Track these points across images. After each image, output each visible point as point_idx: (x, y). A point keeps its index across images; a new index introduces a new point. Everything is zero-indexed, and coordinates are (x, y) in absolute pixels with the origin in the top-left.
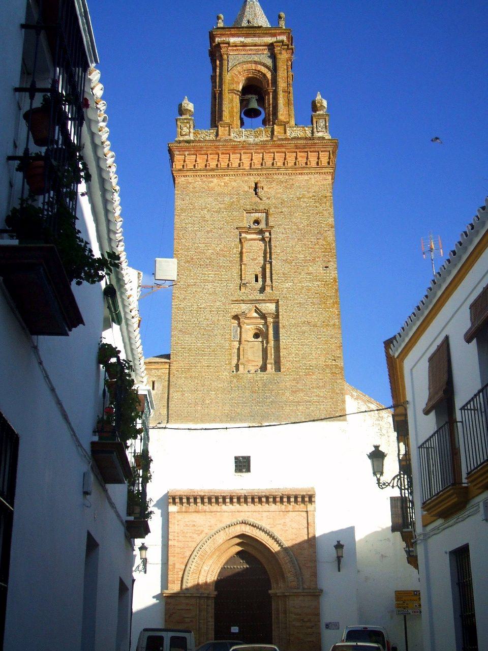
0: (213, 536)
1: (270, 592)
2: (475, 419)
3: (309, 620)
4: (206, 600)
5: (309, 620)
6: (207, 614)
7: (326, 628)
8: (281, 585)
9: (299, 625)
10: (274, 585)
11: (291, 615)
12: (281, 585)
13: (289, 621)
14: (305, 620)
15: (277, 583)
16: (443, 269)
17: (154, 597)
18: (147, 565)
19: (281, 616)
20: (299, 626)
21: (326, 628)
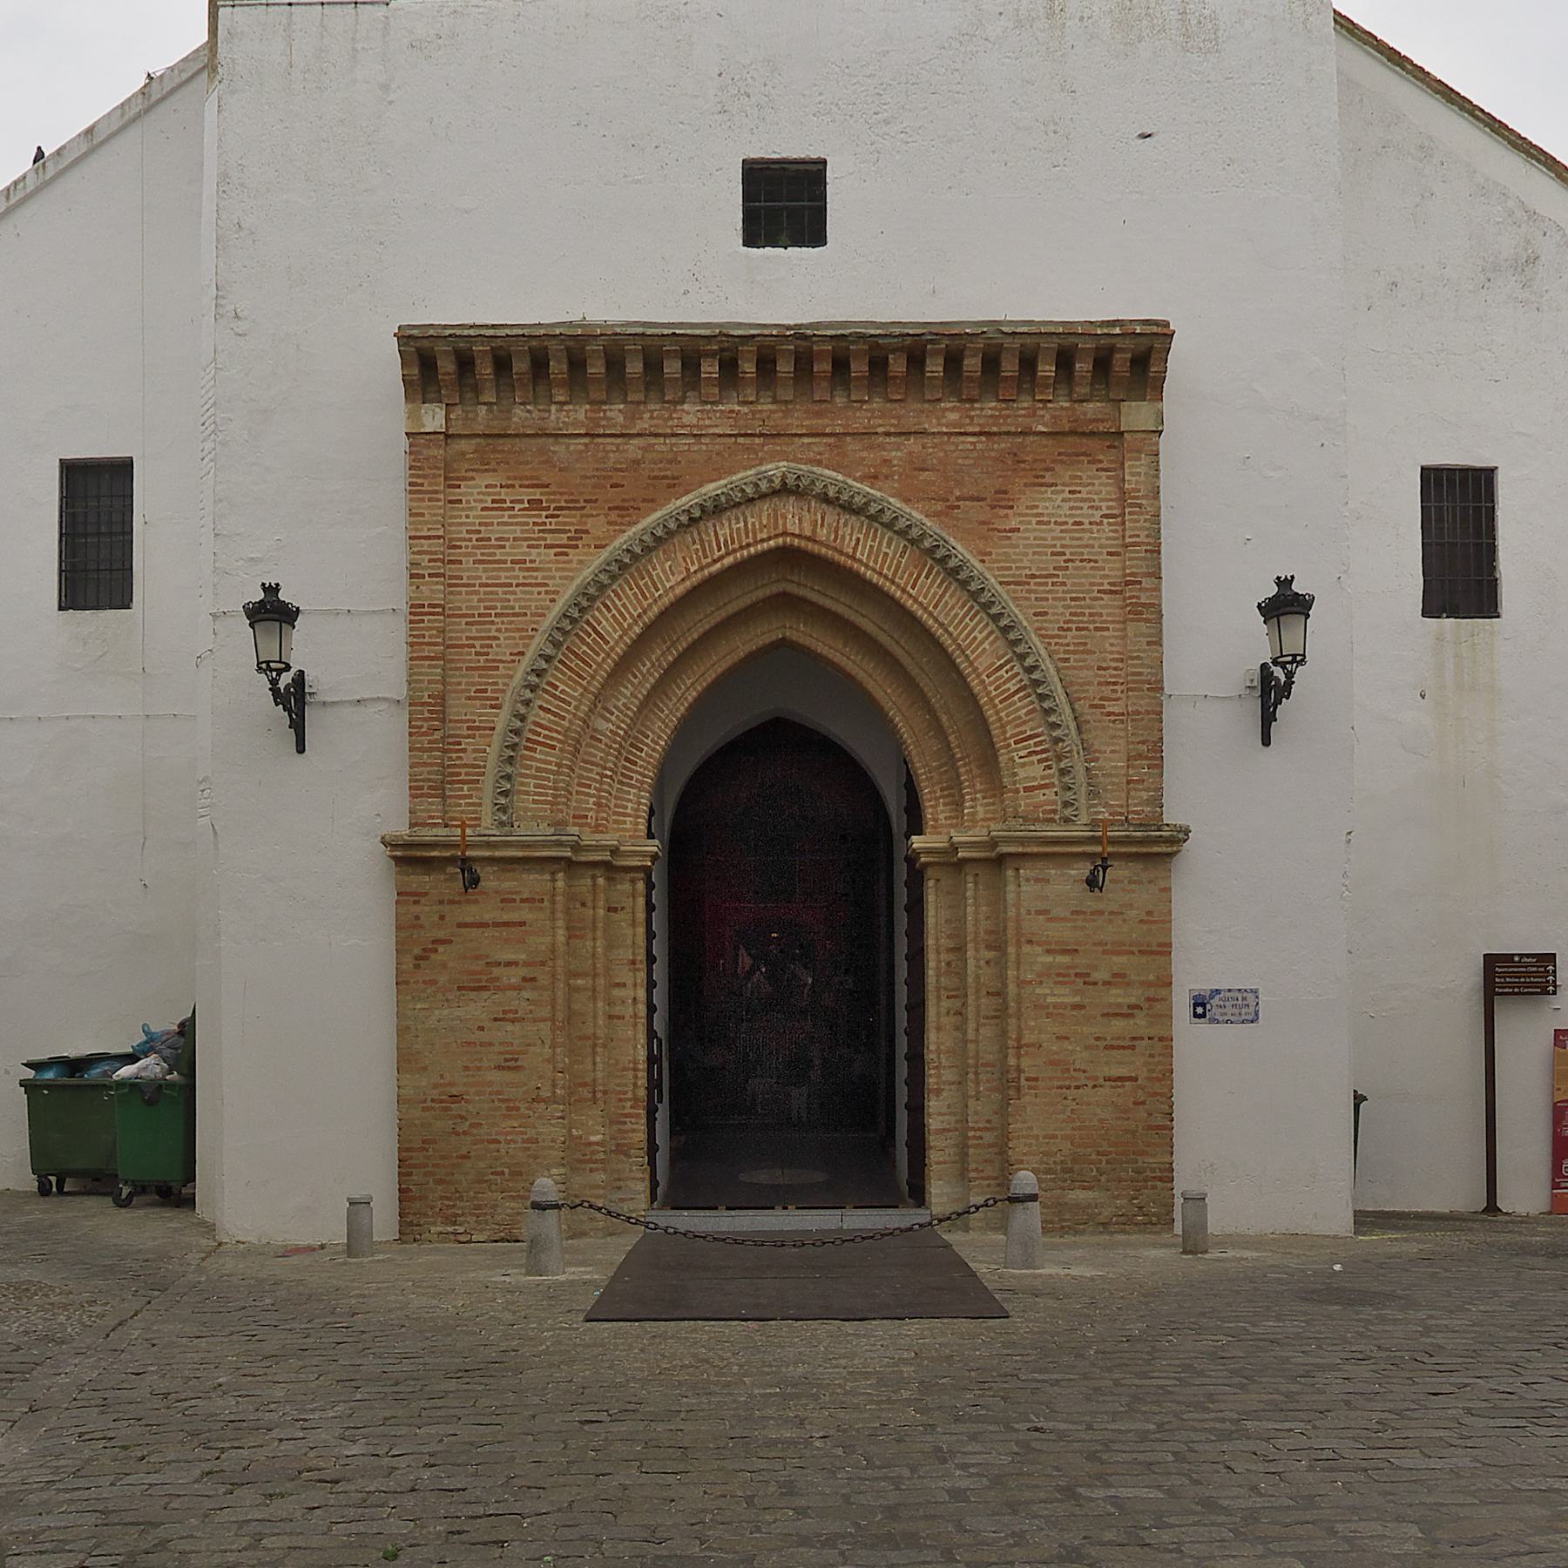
0: (523, 718)
1: (917, 842)
2: (1260, 1340)
3: (1119, 978)
4: (601, 881)
5: (1119, 978)
6: (610, 947)
7: (1196, 1015)
8: (978, 806)
9: (1069, 1000)
10: (935, 809)
11: (1026, 949)
12: (978, 806)
13: (1020, 983)
14: (1096, 976)
15: (958, 804)
16: (624, 496)
17: (28, 1065)
18: (309, 713)
19: (976, 958)
20: (1063, 1006)
21: (1196, 1015)
